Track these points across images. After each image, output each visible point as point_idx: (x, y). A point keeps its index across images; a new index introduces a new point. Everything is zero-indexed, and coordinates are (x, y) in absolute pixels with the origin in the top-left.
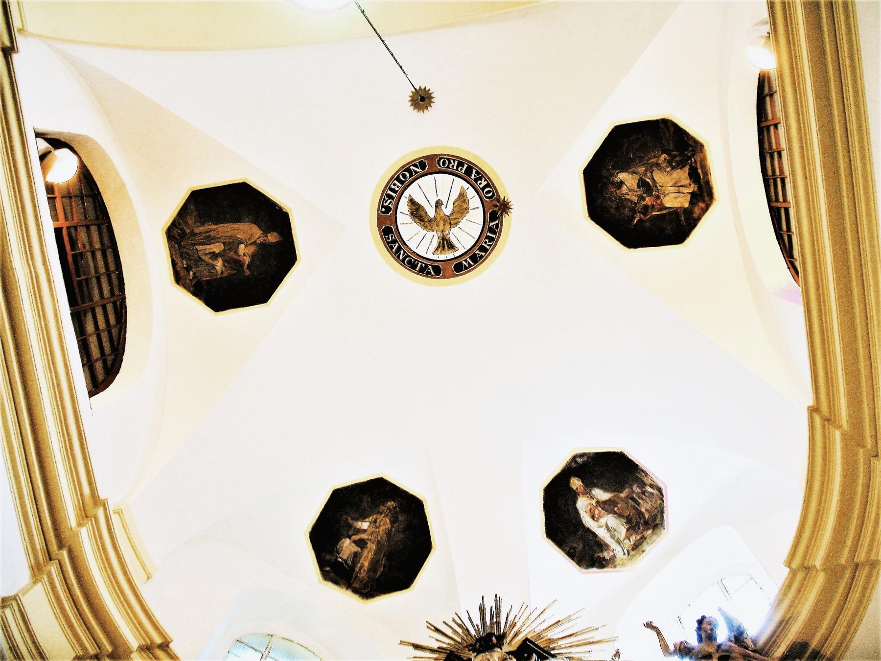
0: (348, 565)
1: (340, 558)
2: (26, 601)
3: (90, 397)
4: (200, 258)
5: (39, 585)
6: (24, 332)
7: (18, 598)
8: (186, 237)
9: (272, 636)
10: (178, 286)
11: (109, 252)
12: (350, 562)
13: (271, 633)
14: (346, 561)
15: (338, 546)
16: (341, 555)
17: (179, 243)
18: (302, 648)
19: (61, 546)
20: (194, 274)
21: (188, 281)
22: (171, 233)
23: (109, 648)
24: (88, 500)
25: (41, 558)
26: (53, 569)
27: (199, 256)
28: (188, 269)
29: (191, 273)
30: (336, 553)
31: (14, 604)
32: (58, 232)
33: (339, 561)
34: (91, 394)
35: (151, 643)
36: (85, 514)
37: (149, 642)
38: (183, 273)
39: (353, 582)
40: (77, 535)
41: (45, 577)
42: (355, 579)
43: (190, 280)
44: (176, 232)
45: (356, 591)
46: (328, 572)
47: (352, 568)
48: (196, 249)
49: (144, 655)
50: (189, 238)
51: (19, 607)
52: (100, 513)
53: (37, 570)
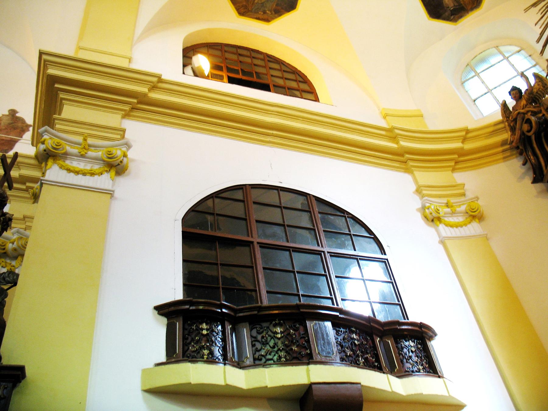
0: (456, 6)
1: (451, 8)
2: (422, 182)
3: (319, 101)
4: (262, 3)
5: (415, 173)
6: (303, 130)
7: (420, 186)
8: (247, 5)
9: (468, 65)
10: (271, 22)
11: (240, 51)
12: (456, 4)
13: (467, 65)
14: (454, 6)
15: (445, 6)
16: (450, 7)
17: (249, 11)
18: (482, 53)
19: (402, 155)
20: (269, 10)
21: (271, 16)
22: (241, 13)
23: (456, 156)
24: (389, 134)
25: (404, 167)
26: (411, 163)
27: (260, 3)
28: (265, 12)
29: (267, 12)
30: (447, 9)
31: (422, 188)
32: (232, 81)
33: (452, 9)
34: (317, 100)
35: (463, 137)
36: (394, 138)
37: (462, 138)
38: (265, 16)
39: (467, 8)
40: (402, 147)
41: (413, 168)
42: (466, 6)
43: (271, 14)
44: (242, 10)
45: (472, 9)
46: (454, 18)
47: (460, 4)
48: (256, 3)
49: (466, 142)
50: (248, 4)
51: (425, 187)
52: (397, 131)
53: (408, 170)
